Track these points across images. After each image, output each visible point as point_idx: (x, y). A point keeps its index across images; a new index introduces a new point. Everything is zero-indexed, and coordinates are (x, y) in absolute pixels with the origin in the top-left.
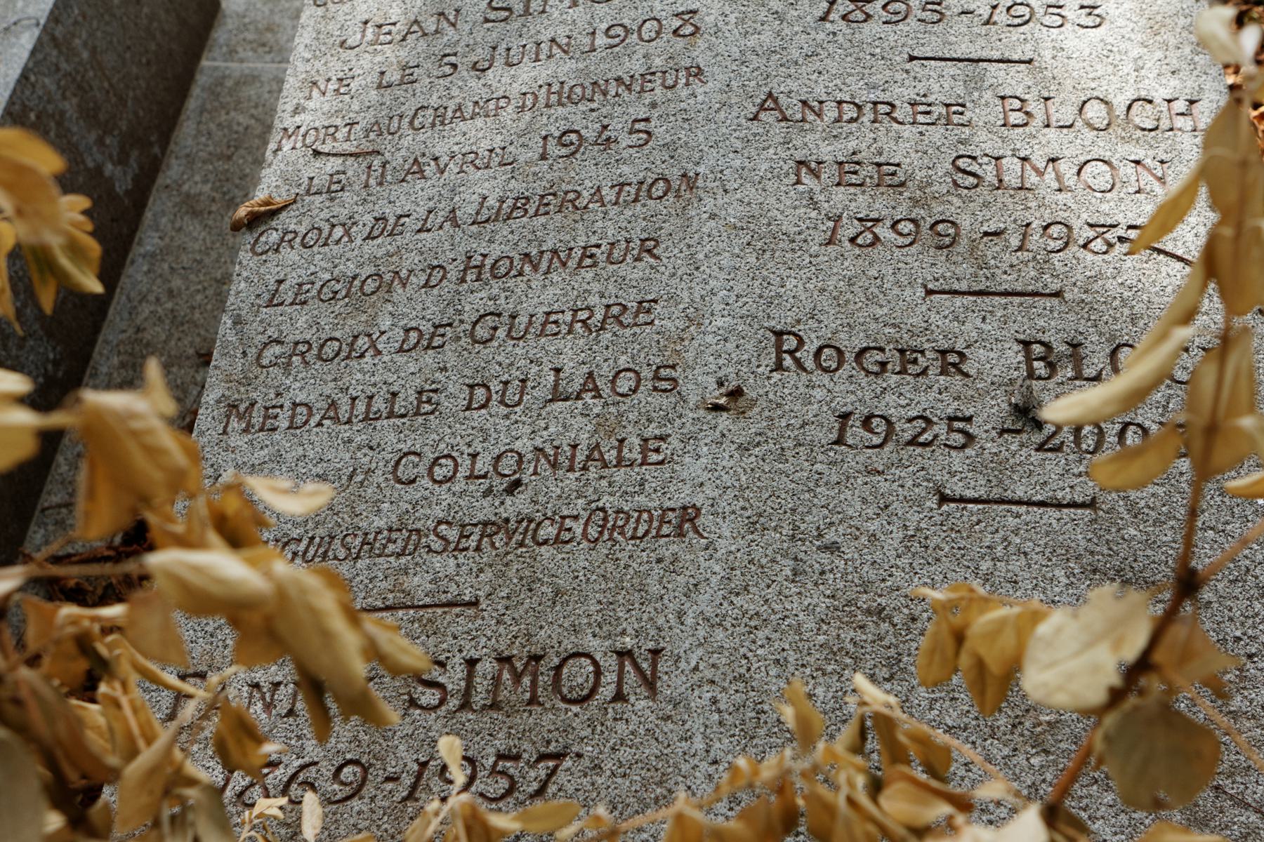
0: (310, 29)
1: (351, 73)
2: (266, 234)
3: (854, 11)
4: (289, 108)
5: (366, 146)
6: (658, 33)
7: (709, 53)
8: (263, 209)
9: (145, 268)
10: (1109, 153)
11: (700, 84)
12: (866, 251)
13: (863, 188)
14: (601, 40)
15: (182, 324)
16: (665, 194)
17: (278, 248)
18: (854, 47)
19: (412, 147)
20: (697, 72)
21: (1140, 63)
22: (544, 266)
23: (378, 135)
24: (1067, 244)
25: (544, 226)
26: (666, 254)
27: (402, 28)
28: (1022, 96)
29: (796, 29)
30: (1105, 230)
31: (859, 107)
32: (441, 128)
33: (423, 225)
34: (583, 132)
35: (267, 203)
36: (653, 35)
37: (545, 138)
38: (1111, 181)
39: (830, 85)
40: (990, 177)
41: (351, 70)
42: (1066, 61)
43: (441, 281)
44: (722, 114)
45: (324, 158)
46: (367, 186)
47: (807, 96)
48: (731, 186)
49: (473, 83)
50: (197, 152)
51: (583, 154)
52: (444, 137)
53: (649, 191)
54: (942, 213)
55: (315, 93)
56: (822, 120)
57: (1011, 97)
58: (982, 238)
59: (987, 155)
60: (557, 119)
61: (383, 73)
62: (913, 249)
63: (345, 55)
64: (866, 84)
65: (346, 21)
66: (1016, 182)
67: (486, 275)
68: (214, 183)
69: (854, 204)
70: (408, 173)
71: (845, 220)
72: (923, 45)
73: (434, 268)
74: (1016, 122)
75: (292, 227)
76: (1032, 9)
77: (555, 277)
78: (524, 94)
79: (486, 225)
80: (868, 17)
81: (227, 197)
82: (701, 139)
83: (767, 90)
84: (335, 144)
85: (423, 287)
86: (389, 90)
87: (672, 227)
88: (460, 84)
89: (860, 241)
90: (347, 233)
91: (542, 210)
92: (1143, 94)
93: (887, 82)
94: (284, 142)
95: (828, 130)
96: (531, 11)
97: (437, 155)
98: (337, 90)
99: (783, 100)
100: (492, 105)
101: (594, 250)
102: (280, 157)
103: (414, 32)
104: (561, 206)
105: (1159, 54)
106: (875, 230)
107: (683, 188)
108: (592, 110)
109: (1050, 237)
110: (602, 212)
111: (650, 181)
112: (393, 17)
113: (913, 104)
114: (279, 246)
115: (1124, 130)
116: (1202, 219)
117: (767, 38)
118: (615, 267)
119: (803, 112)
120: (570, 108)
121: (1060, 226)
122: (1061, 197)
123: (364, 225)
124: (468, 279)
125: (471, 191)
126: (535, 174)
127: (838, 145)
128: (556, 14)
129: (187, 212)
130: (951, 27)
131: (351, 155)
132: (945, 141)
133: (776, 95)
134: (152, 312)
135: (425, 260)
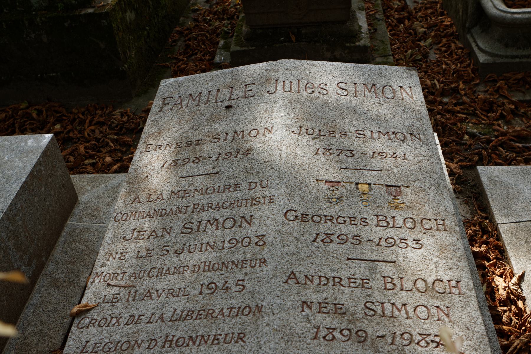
0: (112, 231)
1: (126, 251)
2: (84, 320)
3: (326, 238)
4: (100, 264)
5: (130, 283)
6: (249, 243)
7: (269, 253)
8: (84, 308)
9: (32, 311)
10: (426, 303)
11: (265, 266)
12: (329, 343)
13: (329, 314)
14: (227, 245)
15: (45, 336)
16: (249, 313)
17: (88, 326)
18: (326, 253)
19: (148, 285)
20: (264, 261)
21: (437, 265)
22: (198, 343)
23: (134, 279)
24: (410, 342)
25: (199, 324)
26: (248, 341)
27: (149, 233)
28: (392, 277)
29: (303, 245)
30: (426, 336)
31: (328, 279)
32: (160, 277)
33: (149, 320)
34: (217, 284)
35: (86, 306)
36: (247, 244)
37: (202, 285)
38: (427, 315)
39: (316, 269)
40: (379, 312)
41: (126, 249)
42: (408, 262)
43: (155, 346)
44: (273, 280)
45: (112, 287)
46: (128, 301)
47: (307, 273)
48: (276, 311)
49: (175, 259)
50: (60, 260)
51: (217, 293)
52: (161, 281)
53: (242, 312)
54: (360, 327)
55: (111, 258)
56: (313, 284)
57: (387, 277)
58: (376, 338)
59: (378, 302)
60: (207, 277)
61: (139, 252)
62: (349, 342)
63: (125, 243)
64: (330, 269)
65: (126, 228)
66: (390, 314)
67: (174, 345)
68: (66, 274)
69: (325, 321)
70: (145, 296)
71: (321, 329)
72: (353, 253)
73: (152, 340)
74: (390, 288)
75: (95, 317)
76: (395, 240)
77: (202, 348)
78: (195, 265)
79: (175, 322)
80: (332, 241)
81: (71, 280)
82: (264, 290)
83: (291, 270)
84: (116, 281)
85: (147, 349)
86: (141, 259)
87: (251, 329)
88: (170, 259)
89: (327, 338)
90: (118, 321)
91: (199, 317)
92: (439, 277)
93: (339, 269)
94: (96, 278)
95: (315, 288)
96: (200, 230)
97: (158, 289)
98: (120, 258)
99: (298, 275)
100: (181, 269)
101: (219, 337)
102: (93, 285)
103: (153, 235)
104: (207, 316)
105: (444, 261)
106: (334, 333)
107: (256, 311)
108: (222, 274)
109: (404, 339)
110: (223, 320)
111: (243, 307)
112: (145, 228)
113: (349, 278)
114: (89, 325)
115: (432, 293)
116: (464, 333)
117: (292, 248)
118: (227, 345)
119: (305, 280)
120: (213, 273)
121: (408, 334)
122: (408, 321)
123: (125, 318)
124: (166, 346)
125: (170, 306)
126: (197, 301)
127: (319, 295)
128: (210, 232)
129: (53, 286)
130: (364, 247)
131: (123, 287)
132: (361, 295)
133: (295, 272)
134: (32, 330)
135: (149, 336)
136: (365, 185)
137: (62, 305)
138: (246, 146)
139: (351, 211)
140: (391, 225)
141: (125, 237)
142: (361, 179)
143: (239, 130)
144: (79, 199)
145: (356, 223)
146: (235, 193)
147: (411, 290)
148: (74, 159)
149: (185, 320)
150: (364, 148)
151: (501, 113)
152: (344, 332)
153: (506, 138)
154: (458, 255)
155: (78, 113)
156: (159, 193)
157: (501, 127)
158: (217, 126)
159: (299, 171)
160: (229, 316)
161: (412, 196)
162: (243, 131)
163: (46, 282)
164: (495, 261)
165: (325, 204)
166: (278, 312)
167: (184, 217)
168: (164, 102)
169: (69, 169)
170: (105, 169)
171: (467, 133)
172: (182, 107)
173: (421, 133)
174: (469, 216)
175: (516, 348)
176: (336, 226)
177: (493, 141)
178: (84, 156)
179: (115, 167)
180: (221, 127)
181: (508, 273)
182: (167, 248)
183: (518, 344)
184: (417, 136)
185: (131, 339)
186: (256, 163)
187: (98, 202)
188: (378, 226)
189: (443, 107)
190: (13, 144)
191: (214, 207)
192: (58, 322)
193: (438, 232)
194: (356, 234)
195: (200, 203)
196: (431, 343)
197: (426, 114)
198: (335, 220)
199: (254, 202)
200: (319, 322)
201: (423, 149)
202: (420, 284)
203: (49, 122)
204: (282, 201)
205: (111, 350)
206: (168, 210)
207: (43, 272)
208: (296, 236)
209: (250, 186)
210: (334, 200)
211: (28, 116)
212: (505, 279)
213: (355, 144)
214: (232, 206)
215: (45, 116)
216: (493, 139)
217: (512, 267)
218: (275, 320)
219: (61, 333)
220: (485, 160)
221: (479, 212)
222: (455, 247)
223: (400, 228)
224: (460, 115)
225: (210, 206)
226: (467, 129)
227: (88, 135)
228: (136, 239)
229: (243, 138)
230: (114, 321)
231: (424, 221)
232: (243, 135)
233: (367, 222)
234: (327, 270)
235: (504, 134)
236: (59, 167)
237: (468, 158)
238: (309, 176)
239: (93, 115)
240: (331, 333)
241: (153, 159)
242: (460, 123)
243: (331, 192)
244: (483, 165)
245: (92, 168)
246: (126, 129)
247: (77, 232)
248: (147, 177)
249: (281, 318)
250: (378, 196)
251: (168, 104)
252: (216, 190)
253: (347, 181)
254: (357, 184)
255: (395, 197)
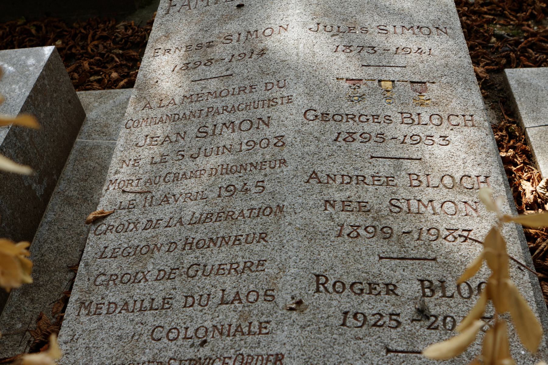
0: (123, 138)
4: (113, 171)
6: (268, 145)
8: (100, 215)
9: (47, 228)
10: (453, 199)
12: (354, 240)
14: (244, 147)
16: (270, 214)
20: (284, 162)
22: (219, 244)
24: (437, 237)
25: (219, 226)
26: (270, 240)
29: (324, 144)
31: (351, 178)
34: (236, 186)
35: (102, 213)
37: (220, 188)
40: (405, 208)
43: (175, 249)
44: (294, 180)
46: (144, 206)
51: (236, 195)
53: (263, 212)
54: (386, 223)
55: (124, 165)
56: (335, 183)
59: (403, 199)
61: (153, 158)
62: (374, 239)
66: (416, 211)
69: (349, 219)
71: (345, 226)
72: (376, 152)
73: (172, 243)
75: (112, 223)
76: (420, 137)
78: (212, 169)
80: (354, 140)
82: (285, 190)
86: (155, 165)
89: (351, 235)
90: (135, 227)
92: (467, 173)
94: (110, 186)
98: (133, 165)
99: (319, 174)
100: (198, 173)
101: (240, 237)
102: (108, 193)
104: (226, 218)
105: (473, 157)
106: (358, 231)
107: (278, 211)
108: (240, 177)
109: (431, 234)
111: (264, 208)
113: (373, 177)
114: (106, 231)
117: (313, 148)
118: (249, 245)
119: (328, 180)
120: (231, 175)
121: (434, 230)
122: (434, 217)
123: (143, 223)
124: (186, 248)
126: (216, 203)
127: (342, 194)
128: (226, 135)
131: (138, 193)
136: (388, 82)
137: (77, 222)
138: (261, 46)
139: (374, 109)
140: (416, 122)
141: (137, 144)
142: (384, 76)
143: (252, 30)
144: (87, 116)
145: (379, 121)
146: (251, 94)
147: (438, 187)
148: (79, 76)
149: (204, 222)
150: (387, 44)
151: (532, 13)
152: (368, 229)
153: (536, 39)
154: (487, 151)
155: (79, 27)
156: (171, 98)
157: (531, 28)
158: (229, 26)
159: (318, 70)
160: (249, 217)
161: (439, 92)
162: (257, 31)
163: (59, 200)
164: (522, 165)
165: (346, 103)
166: (300, 211)
167: (198, 121)
168: (170, 3)
169: (74, 86)
170: (113, 85)
171: (495, 35)
172: (190, 9)
173: (448, 26)
174: (495, 122)
175: (542, 250)
176: (358, 125)
177: (522, 42)
178: (89, 72)
179: (122, 83)
180: (233, 27)
181: (536, 177)
182: (182, 153)
183: (545, 246)
184: (444, 30)
185: (150, 243)
186: (272, 62)
187: (107, 118)
188: (402, 123)
189: (468, 9)
190: (14, 58)
191: (229, 109)
192: (74, 239)
193: (466, 128)
194: (379, 132)
195: (214, 106)
196: (459, 238)
197: (453, 6)
198: (357, 119)
199: (271, 103)
200: (343, 220)
201: (450, 43)
202: (447, 181)
203: (50, 38)
204: (301, 101)
205: (131, 255)
206: (181, 115)
207: (56, 190)
208: (316, 135)
209: (266, 87)
210: (356, 98)
211: (28, 33)
212: (533, 183)
213: (377, 40)
214: (248, 108)
215: (44, 32)
216: (522, 40)
217: (540, 171)
218: (297, 219)
219: (78, 249)
220: (514, 63)
221: (506, 116)
222: (484, 143)
223: (426, 124)
224: (487, 16)
225: (225, 109)
226: (494, 30)
227: (92, 50)
228: (149, 145)
229: (257, 37)
230: (132, 226)
231: (451, 117)
232: (257, 35)
233: (391, 120)
234: (349, 168)
235: (534, 35)
236: (63, 82)
237: (495, 61)
238: (328, 74)
239: (95, 29)
240: (355, 230)
241: (162, 64)
242: (487, 24)
243: (353, 90)
244: (511, 68)
245: (98, 85)
246: (131, 42)
247: (87, 149)
248: (157, 82)
249: (304, 217)
250: (403, 93)
251: (175, 5)
252: (231, 93)
253: (370, 78)
254: (380, 81)
255: (421, 93)
